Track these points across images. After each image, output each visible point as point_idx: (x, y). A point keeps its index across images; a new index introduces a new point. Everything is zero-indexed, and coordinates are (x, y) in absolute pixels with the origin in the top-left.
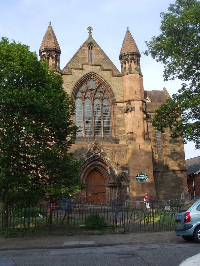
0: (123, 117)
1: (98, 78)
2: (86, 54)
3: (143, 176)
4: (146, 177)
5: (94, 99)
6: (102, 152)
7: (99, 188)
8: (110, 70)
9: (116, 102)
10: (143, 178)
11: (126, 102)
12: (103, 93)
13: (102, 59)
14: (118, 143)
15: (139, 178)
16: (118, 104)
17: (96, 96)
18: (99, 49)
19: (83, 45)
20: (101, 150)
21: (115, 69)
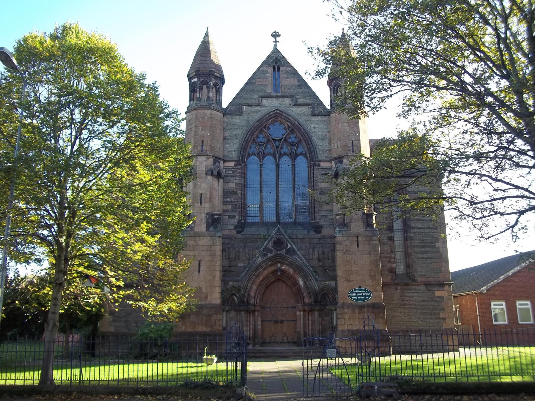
1: (288, 120)
3: (362, 293)
4: (369, 294)
5: (281, 155)
9: (318, 161)
10: (363, 296)
11: (335, 159)
15: (354, 296)
16: (322, 164)
17: (283, 151)
18: (290, 69)
19: (265, 63)
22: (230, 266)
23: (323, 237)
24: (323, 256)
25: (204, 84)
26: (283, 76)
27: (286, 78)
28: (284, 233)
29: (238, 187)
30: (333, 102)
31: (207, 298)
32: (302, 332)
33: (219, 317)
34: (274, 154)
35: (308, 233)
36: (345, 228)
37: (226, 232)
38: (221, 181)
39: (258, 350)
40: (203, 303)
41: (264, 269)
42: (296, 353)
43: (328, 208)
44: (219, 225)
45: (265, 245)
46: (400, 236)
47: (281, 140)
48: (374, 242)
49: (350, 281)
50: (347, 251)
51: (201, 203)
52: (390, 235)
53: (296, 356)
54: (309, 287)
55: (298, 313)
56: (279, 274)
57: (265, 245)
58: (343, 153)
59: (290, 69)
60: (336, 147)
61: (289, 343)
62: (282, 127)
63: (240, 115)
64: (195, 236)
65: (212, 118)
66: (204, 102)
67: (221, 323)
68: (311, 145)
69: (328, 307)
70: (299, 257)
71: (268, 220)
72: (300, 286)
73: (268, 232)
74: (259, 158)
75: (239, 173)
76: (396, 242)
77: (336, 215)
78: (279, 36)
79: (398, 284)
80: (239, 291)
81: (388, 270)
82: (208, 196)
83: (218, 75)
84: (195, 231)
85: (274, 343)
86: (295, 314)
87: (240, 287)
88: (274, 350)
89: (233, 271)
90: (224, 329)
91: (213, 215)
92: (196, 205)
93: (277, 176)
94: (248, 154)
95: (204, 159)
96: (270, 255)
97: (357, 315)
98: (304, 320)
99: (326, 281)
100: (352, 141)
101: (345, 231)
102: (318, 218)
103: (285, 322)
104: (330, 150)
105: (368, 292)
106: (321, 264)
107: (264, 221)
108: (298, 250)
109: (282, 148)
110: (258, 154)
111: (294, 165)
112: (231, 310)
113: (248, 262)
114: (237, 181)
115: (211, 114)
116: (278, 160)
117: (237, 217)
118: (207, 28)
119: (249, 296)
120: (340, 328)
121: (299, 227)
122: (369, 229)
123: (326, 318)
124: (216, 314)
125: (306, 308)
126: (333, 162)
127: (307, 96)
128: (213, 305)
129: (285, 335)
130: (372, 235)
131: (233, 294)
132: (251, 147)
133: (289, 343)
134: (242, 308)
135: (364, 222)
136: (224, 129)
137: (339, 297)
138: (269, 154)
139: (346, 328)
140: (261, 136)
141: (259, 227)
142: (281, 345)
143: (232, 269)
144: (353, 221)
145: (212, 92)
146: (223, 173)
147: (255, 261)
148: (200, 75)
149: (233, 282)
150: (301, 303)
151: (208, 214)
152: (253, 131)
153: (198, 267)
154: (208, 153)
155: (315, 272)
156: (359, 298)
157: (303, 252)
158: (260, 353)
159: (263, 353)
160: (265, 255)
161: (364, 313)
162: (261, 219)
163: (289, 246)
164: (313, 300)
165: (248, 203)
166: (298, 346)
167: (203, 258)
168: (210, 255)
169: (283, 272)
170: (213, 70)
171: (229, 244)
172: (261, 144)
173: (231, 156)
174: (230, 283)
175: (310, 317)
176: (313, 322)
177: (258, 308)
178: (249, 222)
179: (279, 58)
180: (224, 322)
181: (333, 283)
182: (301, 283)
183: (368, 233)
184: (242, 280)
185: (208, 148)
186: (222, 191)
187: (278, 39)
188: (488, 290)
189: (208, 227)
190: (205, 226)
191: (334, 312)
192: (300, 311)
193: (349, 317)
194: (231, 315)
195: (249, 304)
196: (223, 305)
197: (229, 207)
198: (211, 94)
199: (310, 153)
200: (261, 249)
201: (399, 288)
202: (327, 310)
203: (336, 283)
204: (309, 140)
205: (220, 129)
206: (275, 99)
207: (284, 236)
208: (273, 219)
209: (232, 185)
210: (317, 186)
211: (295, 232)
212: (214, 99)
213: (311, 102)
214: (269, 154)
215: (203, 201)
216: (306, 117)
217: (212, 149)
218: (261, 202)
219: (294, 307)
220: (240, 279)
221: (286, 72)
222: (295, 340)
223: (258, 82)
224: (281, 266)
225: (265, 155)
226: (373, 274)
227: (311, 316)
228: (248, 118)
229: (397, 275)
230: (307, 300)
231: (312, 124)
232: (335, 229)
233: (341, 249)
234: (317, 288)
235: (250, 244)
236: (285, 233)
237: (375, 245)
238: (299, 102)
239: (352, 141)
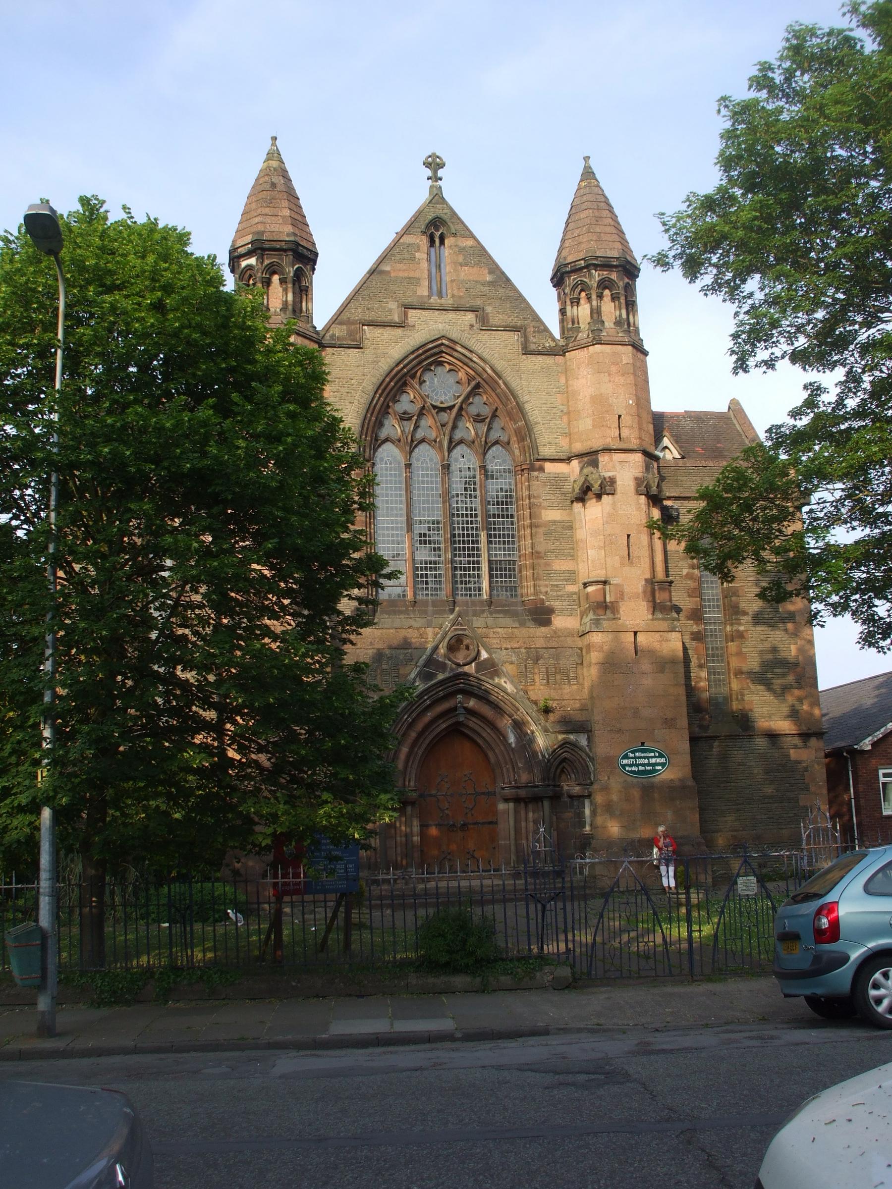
0: (567, 518)
1: (466, 362)
3: (648, 758)
4: (662, 760)
5: (453, 445)
6: (482, 658)
8: (515, 329)
9: (538, 460)
10: (649, 765)
11: (579, 456)
14: (547, 622)
15: (630, 766)
16: (548, 466)
17: (458, 435)
18: (470, 242)
21: (537, 324)
23: (556, 634)
47: (451, 408)
52: (695, 629)
59: (470, 242)
62: (451, 379)
63: (358, 347)
78: (442, 166)
98: (517, 821)
101: (608, 619)
105: (661, 756)
116: (446, 454)
156: (641, 768)
179: (445, 217)
187: (440, 173)
188: (874, 745)
210: (540, 517)
216: (509, 356)
221: (462, 250)
239: (620, 416)
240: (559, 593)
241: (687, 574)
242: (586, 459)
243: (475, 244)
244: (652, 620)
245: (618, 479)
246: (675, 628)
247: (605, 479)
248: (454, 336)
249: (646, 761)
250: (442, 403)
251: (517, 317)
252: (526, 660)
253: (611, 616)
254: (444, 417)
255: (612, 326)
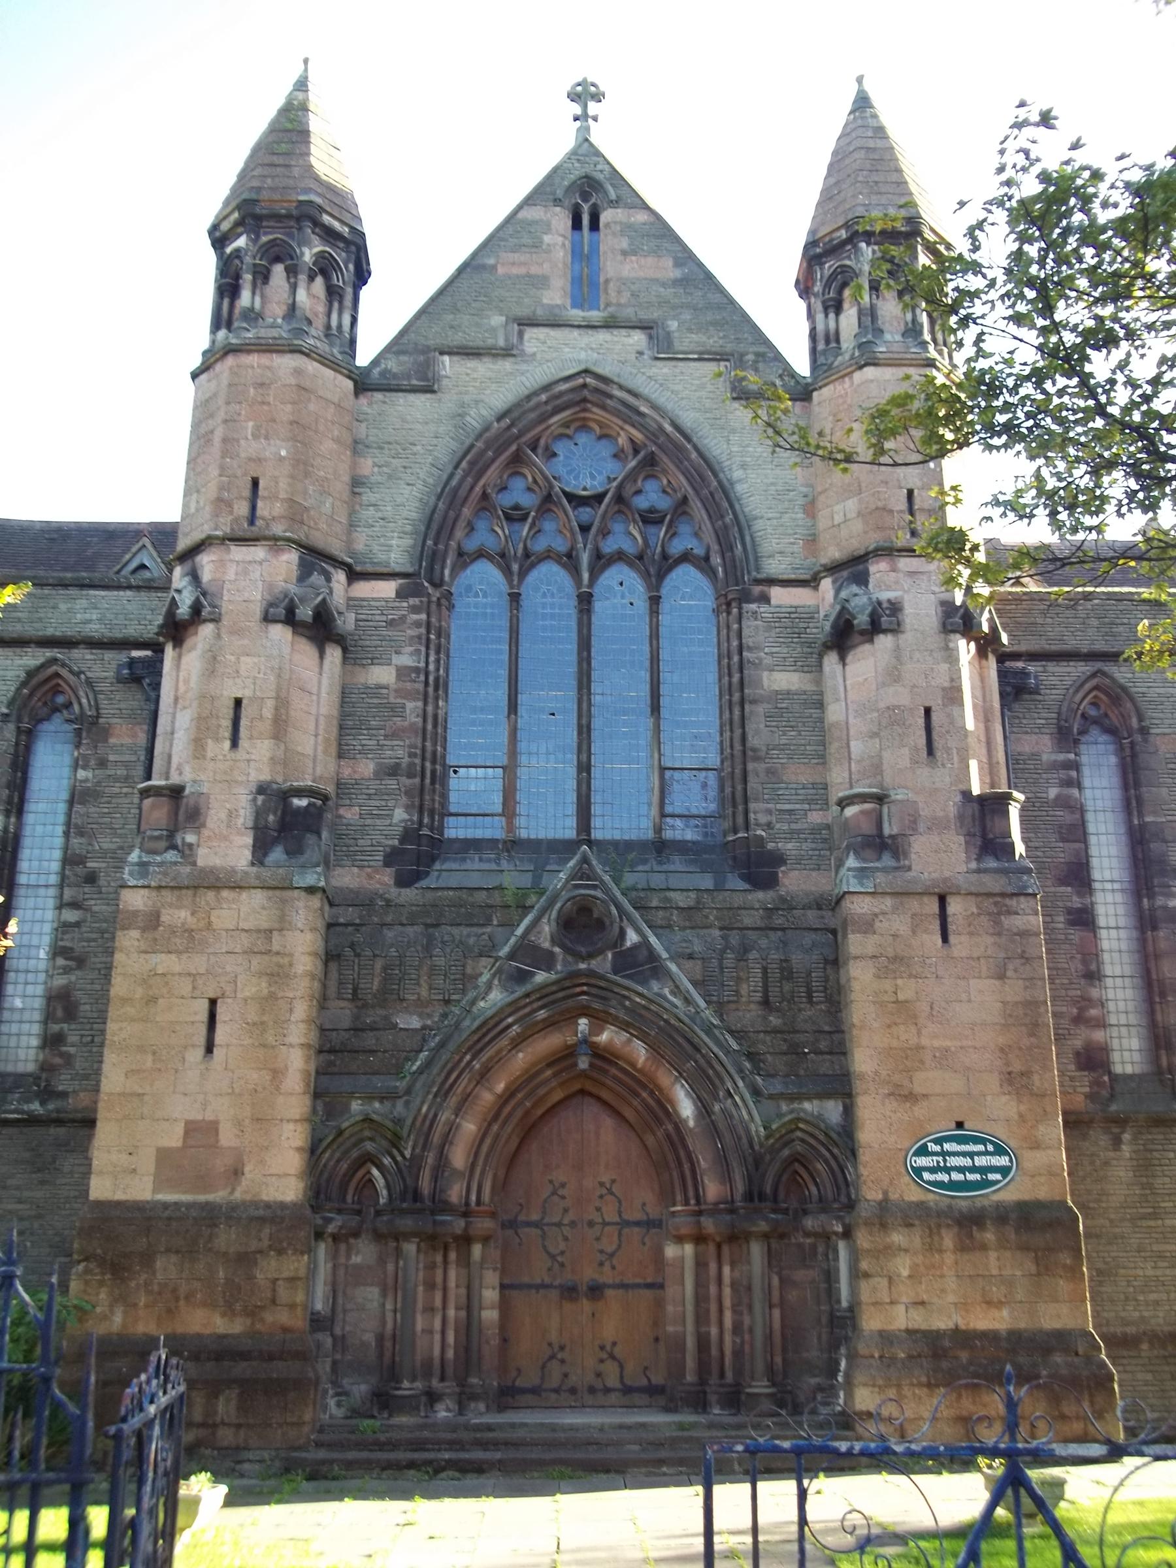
0: (810, 687)
1: (631, 414)
2: (548, 252)
3: (971, 1155)
4: (1003, 1161)
5: (601, 562)
6: (628, 944)
7: (610, 1250)
8: (719, 357)
9: (758, 582)
10: (974, 1169)
11: (833, 569)
12: (668, 517)
13: (664, 285)
14: (767, 881)
15: (933, 1170)
16: (778, 595)
17: (609, 546)
18: (641, 217)
19: (540, 195)
20: (622, 934)
21: (762, 349)
22: (357, 1030)
23: (786, 905)
24: (787, 987)
25: (278, 259)
26: (610, 242)
27: (624, 253)
28: (606, 878)
29: (409, 685)
30: (821, 346)
31: (237, 1172)
32: (690, 1343)
33: (295, 1265)
34: (569, 555)
35: (719, 888)
36: (887, 860)
37: (347, 878)
38: (334, 654)
39: (478, 1428)
40: (217, 1196)
41: (516, 1044)
42: (660, 1445)
43: (803, 779)
44: (311, 839)
45: (519, 931)
46: (1121, 910)
47: (599, 498)
48: (1018, 922)
49: (911, 1098)
50: (896, 959)
51: (235, 744)
52: (1076, 902)
53: (661, 1462)
54: (721, 1125)
55: (671, 1251)
56: (583, 1063)
57: (519, 931)
58: (872, 540)
60: (838, 519)
61: (627, 1390)
63: (429, 390)
64: (196, 887)
65: (300, 387)
66: (273, 326)
67: (300, 1297)
68: (729, 518)
69: (809, 1223)
70: (677, 990)
71: (542, 836)
72: (678, 1124)
73: (537, 879)
74: (507, 571)
75: (417, 624)
76: (1103, 933)
77: (843, 803)
78: (598, 97)
79: (1121, 1122)
80: (396, 1142)
81: (1078, 1054)
82: (268, 712)
83: (337, 225)
84: (200, 862)
85: (556, 1391)
86: (659, 1252)
87: (399, 1121)
88: (553, 1428)
89: (372, 1052)
90: (318, 1322)
91: (286, 795)
92: (211, 748)
93: (585, 645)
94: (461, 554)
95: (258, 552)
96: (541, 977)
97: (949, 1258)
98: (700, 1284)
99: (800, 1097)
100: (910, 493)
101: (884, 870)
102: (763, 819)
103: (609, 1293)
104: (812, 540)
105: (1000, 1151)
106: (775, 1021)
107: (524, 834)
108: (672, 958)
109: (605, 533)
110: (503, 555)
111: (655, 601)
112: (356, 1234)
113: (439, 1010)
114: (406, 659)
115: (298, 372)
116: (586, 576)
117: (400, 814)
118: (306, 61)
119: (442, 1162)
120: (871, 1322)
121: (677, 863)
122: (992, 864)
123: (800, 1275)
124: (281, 1252)
125: (709, 1225)
126: (827, 584)
127: (714, 323)
128: (268, 1206)
129: (612, 1357)
130: (1010, 890)
131: (369, 1159)
132: (471, 528)
133: (627, 1390)
134: (406, 1223)
135: (969, 834)
136: (357, 447)
137: (863, 1171)
138: (549, 555)
139: (901, 1319)
140: (518, 484)
141: (497, 861)
142: (589, 1399)
143: (369, 1040)
144: (922, 827)
145: (310, 294)
146: (347, 622)
147: (473, 1002)
148: (259, 218)
149: (369, 1098)
150: (687, 1203)
151: (262, 789)
152: (482, 453)
153: (203, 1030)
154: (278, 529)
155: (750, 1056)
157: (697, 967)
158: (484, 1445)
159: (496, 1444)
160: (522, 977)
161: (984, 1247)
162: (510, 827)
163: (632, 937)
164: (740, 1187)
165: (451, 760)
166: (667, 1410)
167: (229, 989)
168: (261, 974)
169: (603, 1057)
170: (319, 200)
171: (357, 927)
172: (515, 516)
173: (382, 557)
174: (356, 1106)
175: (726, 1270)
176: (742, 1289)
177: (484, 1225)
178: (457, 840)
179: (600, 177)
180: (321, 1290)
181: (832, 1111)
182: (686, 1109)
183: (993, 883)
184: (408, 1091)
185: (278, 508)
186: (336, 698)
189: (261, 848)
190: (249, 840)
191: (842, 1246)
192: (680, 1239)
193: (914, 1267)
194: (356, 1259)
195: (440, 1205)
196: (315, 1209)
197: (366, 768)
198: (302, 295)
199: (726, 547)
200: (504, 951)
201: (1126, 1137)
202: (807, 1234)
203: (849, 1111)
204: (719, 495)
205: (337, 441)
206: (576, 333)
207: (607, 891)
208: (567, 829)
209: (382, 675)
210: (758, 683)
211: (657, 880)
212: (319, 322)
213: (729, 347)
214: (549, 555)
215: (243, 732)
216: (708, 404)
217: (296, 513)
218: (513, 753)
219: (651, 1224)
220: (401, 1085)
222: (658, 1379)
223: (508, 264)
224: (596, 1029)
225: (530, 560)
226: (1017, 1066)
227: (733, 1264)
228: (462, 405)
229: (1114, 1078)
230: (712, 1190)
231: (733, 431)
232: (840, 864)
233: (870, 950)
234: (757, 1129)
235: (456, 931)
236: (617, 881)
237: (1024, 934)
238: (677, 345)
239: (910, 493)
240: (794, 826)
241: (1058, 797)
242: (845, 574)
243: (652, 219)
244: (979, 871)
245: (908, 610)
246: (1026, 887)
247: (879, 603)
248: (605, 370)
249: (967, 1162)
250: (585, 489)
251: (724, 337)
252: (723, 951)
253: (892, 863)
254: (585, 513)
255: (898, 338)
